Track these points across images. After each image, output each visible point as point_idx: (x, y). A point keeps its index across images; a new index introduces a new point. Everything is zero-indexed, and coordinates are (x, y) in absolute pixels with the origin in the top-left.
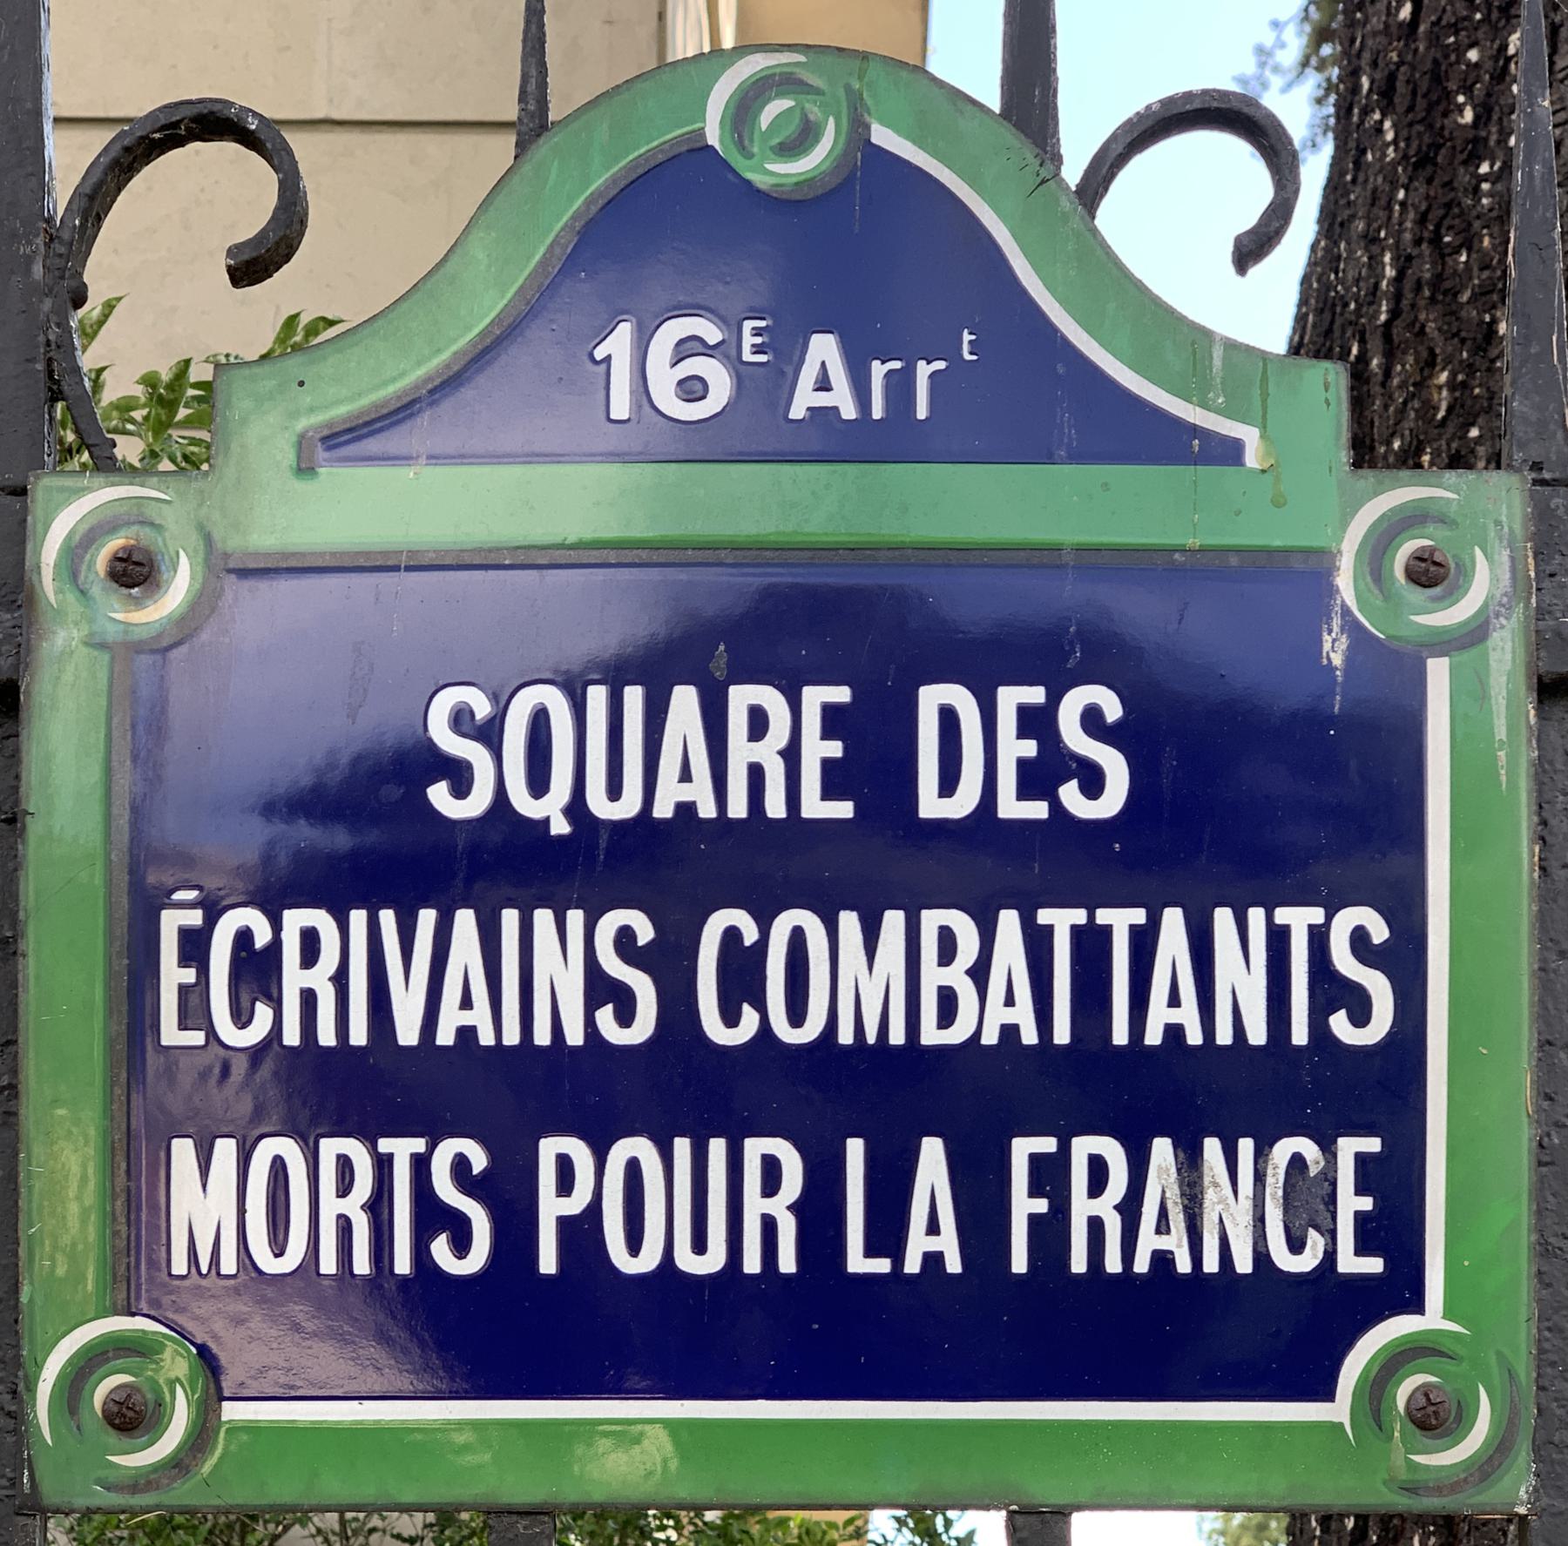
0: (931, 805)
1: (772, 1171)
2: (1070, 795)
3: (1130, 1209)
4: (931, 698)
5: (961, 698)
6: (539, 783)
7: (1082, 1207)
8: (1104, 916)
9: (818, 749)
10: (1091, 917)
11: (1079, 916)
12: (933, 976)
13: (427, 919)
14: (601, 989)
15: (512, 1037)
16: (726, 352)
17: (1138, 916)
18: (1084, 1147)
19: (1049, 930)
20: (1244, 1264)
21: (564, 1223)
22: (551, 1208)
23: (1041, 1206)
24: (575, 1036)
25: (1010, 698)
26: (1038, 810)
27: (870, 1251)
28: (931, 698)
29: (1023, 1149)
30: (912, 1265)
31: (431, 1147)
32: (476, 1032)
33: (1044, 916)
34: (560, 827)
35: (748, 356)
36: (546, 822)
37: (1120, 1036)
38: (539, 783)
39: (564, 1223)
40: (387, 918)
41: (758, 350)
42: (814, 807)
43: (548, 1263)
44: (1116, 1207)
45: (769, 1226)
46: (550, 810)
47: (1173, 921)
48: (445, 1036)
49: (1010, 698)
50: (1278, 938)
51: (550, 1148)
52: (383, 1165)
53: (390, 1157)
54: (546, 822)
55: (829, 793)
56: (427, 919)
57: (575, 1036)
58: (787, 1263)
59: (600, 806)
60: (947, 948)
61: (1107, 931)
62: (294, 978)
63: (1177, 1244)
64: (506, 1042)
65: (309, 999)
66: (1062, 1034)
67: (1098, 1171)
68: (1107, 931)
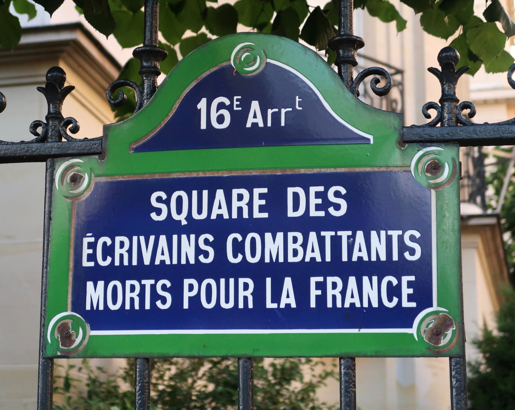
0: (291, 213)
1: (246, 287)
2: (331, 210)
3: (343, 293)
4: (290, 191)
5: (300, 191)
6: (179, 211)
7: (330, 292)
8: (339, 233)
9: (258, 202)
10: (336, 233)
11: (333, 233)
12: (291, 246)
13: (152, 238)
14: (198, 251)
15: (175, 262)
16: (230, 108)
17: (350, 233)
18: (330, 280)
19: (324, 237)
20: (375, 304)
21: (190, 298)
22: (187, 295)
23: (319, 292)
24: (192, 261)
25: (313, 190)
26: (322, 214)
27: (273, 302)
28: (290, 191)
29: (314, 280)
30: (282, 306)
31: (156, 283)
32: (165, 261)
33: (323, 233)
34: (184, 222)
35: (235, 108)
36: (180, 221)
37: (345, 258)
38: (179, 211)
39: (190, 298)
40: (142, 238)
41: (237, 106)
42: (257, 214)
43: (186, 306)
44: (340, 292)
45: (246, 298)
46: (182, 218)
47: (360, 234)
48: (157, 262)
49: (313, 190)
50: (389, 239)
51: (187, 282)
52: (143, 287)
53: (145, 285)
54: (180, 221)
55: (260, 211)
56: (152, 238)
57: (192, 261)
58: (251, 306)
59: (195, 216)
60: (295, 240)
61: (341, 237)
62: (118, 251)
63: (356, 301)
64: (174, 263)
65: (121, 256)
66: (328, 259)
67: (334, 286)
68: (341, 237)
